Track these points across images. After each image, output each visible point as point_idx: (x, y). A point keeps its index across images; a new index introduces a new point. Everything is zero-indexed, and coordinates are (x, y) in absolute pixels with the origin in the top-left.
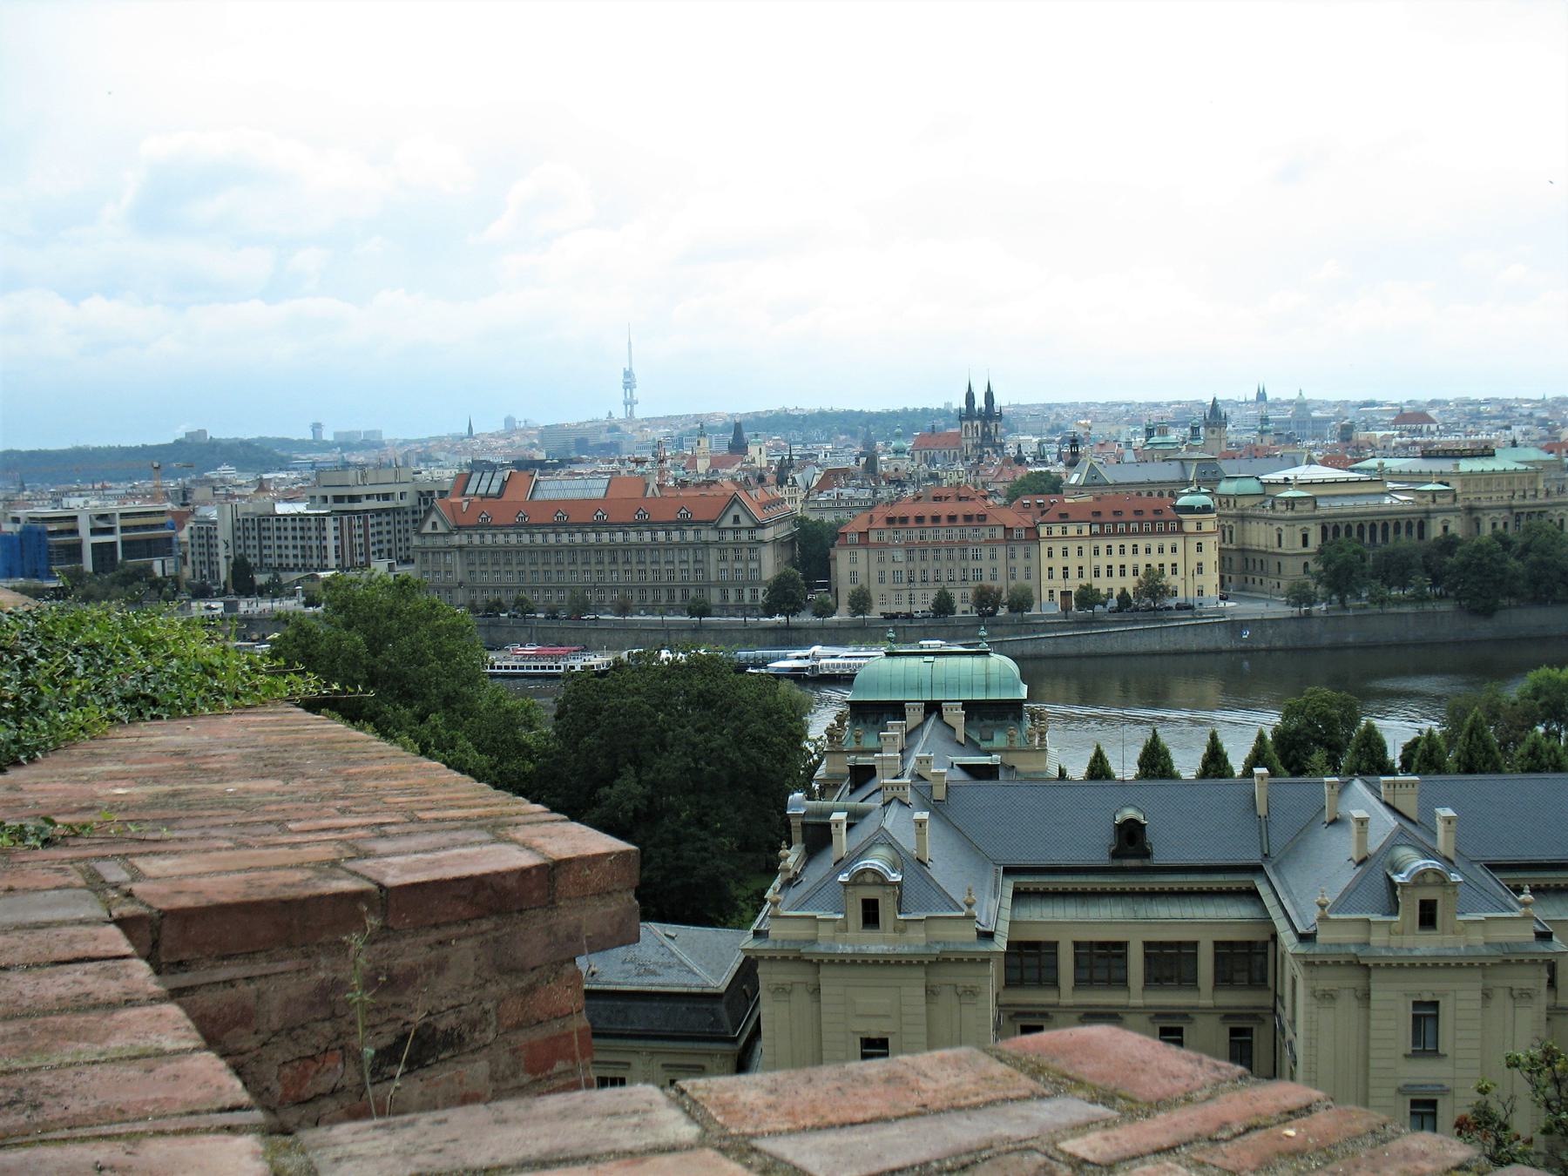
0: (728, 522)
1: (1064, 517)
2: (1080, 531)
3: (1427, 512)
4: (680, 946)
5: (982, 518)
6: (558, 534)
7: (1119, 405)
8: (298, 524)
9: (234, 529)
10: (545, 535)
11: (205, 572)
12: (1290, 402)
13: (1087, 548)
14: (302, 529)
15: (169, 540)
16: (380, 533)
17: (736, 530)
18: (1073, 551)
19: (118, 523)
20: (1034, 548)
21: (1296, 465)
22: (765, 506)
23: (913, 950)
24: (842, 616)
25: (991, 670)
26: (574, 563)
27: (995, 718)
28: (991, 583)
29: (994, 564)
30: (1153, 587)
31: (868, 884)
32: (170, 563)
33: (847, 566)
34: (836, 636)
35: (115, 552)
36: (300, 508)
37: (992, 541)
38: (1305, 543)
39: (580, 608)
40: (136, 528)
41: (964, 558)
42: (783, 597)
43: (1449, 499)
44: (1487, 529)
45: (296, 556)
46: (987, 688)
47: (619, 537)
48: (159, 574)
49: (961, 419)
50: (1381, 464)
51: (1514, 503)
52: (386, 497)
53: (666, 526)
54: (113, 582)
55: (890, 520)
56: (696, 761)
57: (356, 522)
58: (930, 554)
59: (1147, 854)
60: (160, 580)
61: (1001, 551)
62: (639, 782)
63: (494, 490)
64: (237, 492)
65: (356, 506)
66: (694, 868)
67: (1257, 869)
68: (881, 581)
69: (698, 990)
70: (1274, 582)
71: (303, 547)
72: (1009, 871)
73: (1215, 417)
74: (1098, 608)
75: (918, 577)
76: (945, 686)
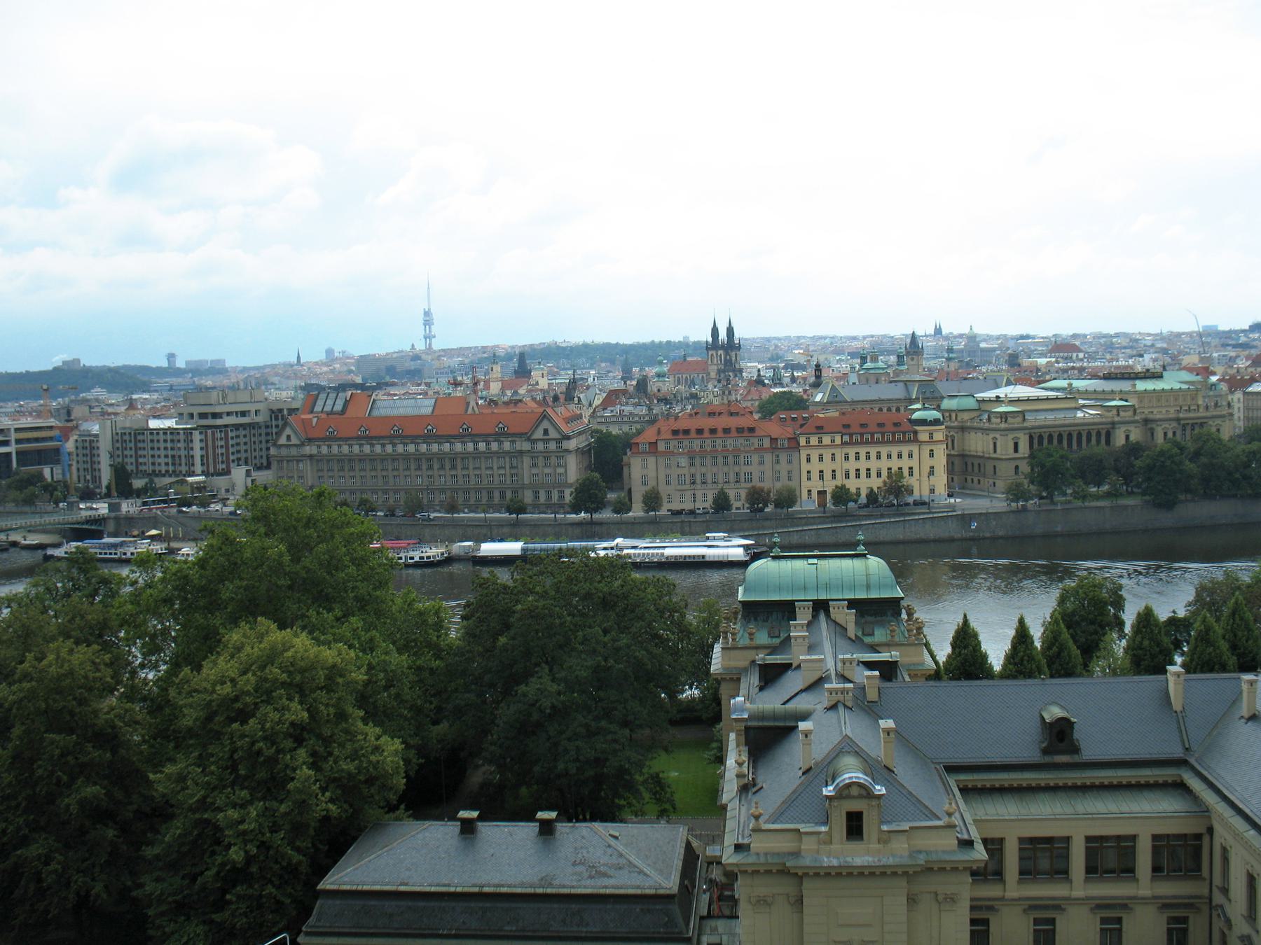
0: (539, 434)
1: (820, 429)
2: (833, 441)
3: (1113, 423)
4: (626, 846)
5: (752, 430)
6: (394, 445)
7: (825, 338)
8: (169, 437)
9: (114, 441)
10: (383, 445)
11: (89, 477)
12: (961, 336)
13: (839, 454)
14: (172, 441)
15: (57, 451)
16: (238, 444)
17: (546, 441)
18: (827, 457)
19: (13, 436)
20: (795, 455)
21: (997, 387)
22: (569, 420)
23: (897, 861)
24: (637, 512)
25: (871, 571)
26: (408, 469)
27: (875, 614)
28: (759, 485)
29: (762, 468)
30: (896, 486)
31: (854, 797)
32: (58, 470)
33: (640, 471)
34: (634, 530)
35: (11, 461)
36: (170, 423)
37: (760, 449)
38: (1016, 450)
39: (414, 507)
40: (28, 440)
41: (737, 463)
42: (587, 498)
43: (1130, 413)
44: (1159, 439)
45: (167, 464)
46: (868, 587)
47: (411, 448)
48: (49, 480)
49: (707, 349)
50: (1070, 385)
51: (1181, 415)
52: (243, 414)
53: (486, 438)
54: (9, 487)
55: (675, 432)
56: (606, 660)
57: (218, 435)
58: (708, 461)
59: (1075, 750)
60: (50, 485)
61: (768, 458)
62: (553, 681)
63: (338, 407)
64: (110, 410)
65: (219, 422)
66: (607, 759)
67: (1182, 763)
68: (668, 483)
69: (652, 892)
70: (991, 481)
71: (173, 456)
72: (951, 769)
73: (913, 347)
74: (851, 505)
75: (698, 479)
76: (828, 587)
